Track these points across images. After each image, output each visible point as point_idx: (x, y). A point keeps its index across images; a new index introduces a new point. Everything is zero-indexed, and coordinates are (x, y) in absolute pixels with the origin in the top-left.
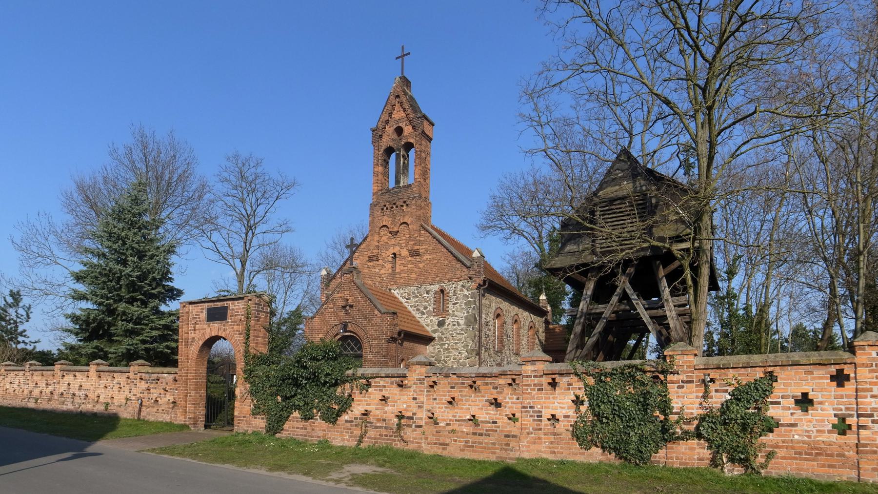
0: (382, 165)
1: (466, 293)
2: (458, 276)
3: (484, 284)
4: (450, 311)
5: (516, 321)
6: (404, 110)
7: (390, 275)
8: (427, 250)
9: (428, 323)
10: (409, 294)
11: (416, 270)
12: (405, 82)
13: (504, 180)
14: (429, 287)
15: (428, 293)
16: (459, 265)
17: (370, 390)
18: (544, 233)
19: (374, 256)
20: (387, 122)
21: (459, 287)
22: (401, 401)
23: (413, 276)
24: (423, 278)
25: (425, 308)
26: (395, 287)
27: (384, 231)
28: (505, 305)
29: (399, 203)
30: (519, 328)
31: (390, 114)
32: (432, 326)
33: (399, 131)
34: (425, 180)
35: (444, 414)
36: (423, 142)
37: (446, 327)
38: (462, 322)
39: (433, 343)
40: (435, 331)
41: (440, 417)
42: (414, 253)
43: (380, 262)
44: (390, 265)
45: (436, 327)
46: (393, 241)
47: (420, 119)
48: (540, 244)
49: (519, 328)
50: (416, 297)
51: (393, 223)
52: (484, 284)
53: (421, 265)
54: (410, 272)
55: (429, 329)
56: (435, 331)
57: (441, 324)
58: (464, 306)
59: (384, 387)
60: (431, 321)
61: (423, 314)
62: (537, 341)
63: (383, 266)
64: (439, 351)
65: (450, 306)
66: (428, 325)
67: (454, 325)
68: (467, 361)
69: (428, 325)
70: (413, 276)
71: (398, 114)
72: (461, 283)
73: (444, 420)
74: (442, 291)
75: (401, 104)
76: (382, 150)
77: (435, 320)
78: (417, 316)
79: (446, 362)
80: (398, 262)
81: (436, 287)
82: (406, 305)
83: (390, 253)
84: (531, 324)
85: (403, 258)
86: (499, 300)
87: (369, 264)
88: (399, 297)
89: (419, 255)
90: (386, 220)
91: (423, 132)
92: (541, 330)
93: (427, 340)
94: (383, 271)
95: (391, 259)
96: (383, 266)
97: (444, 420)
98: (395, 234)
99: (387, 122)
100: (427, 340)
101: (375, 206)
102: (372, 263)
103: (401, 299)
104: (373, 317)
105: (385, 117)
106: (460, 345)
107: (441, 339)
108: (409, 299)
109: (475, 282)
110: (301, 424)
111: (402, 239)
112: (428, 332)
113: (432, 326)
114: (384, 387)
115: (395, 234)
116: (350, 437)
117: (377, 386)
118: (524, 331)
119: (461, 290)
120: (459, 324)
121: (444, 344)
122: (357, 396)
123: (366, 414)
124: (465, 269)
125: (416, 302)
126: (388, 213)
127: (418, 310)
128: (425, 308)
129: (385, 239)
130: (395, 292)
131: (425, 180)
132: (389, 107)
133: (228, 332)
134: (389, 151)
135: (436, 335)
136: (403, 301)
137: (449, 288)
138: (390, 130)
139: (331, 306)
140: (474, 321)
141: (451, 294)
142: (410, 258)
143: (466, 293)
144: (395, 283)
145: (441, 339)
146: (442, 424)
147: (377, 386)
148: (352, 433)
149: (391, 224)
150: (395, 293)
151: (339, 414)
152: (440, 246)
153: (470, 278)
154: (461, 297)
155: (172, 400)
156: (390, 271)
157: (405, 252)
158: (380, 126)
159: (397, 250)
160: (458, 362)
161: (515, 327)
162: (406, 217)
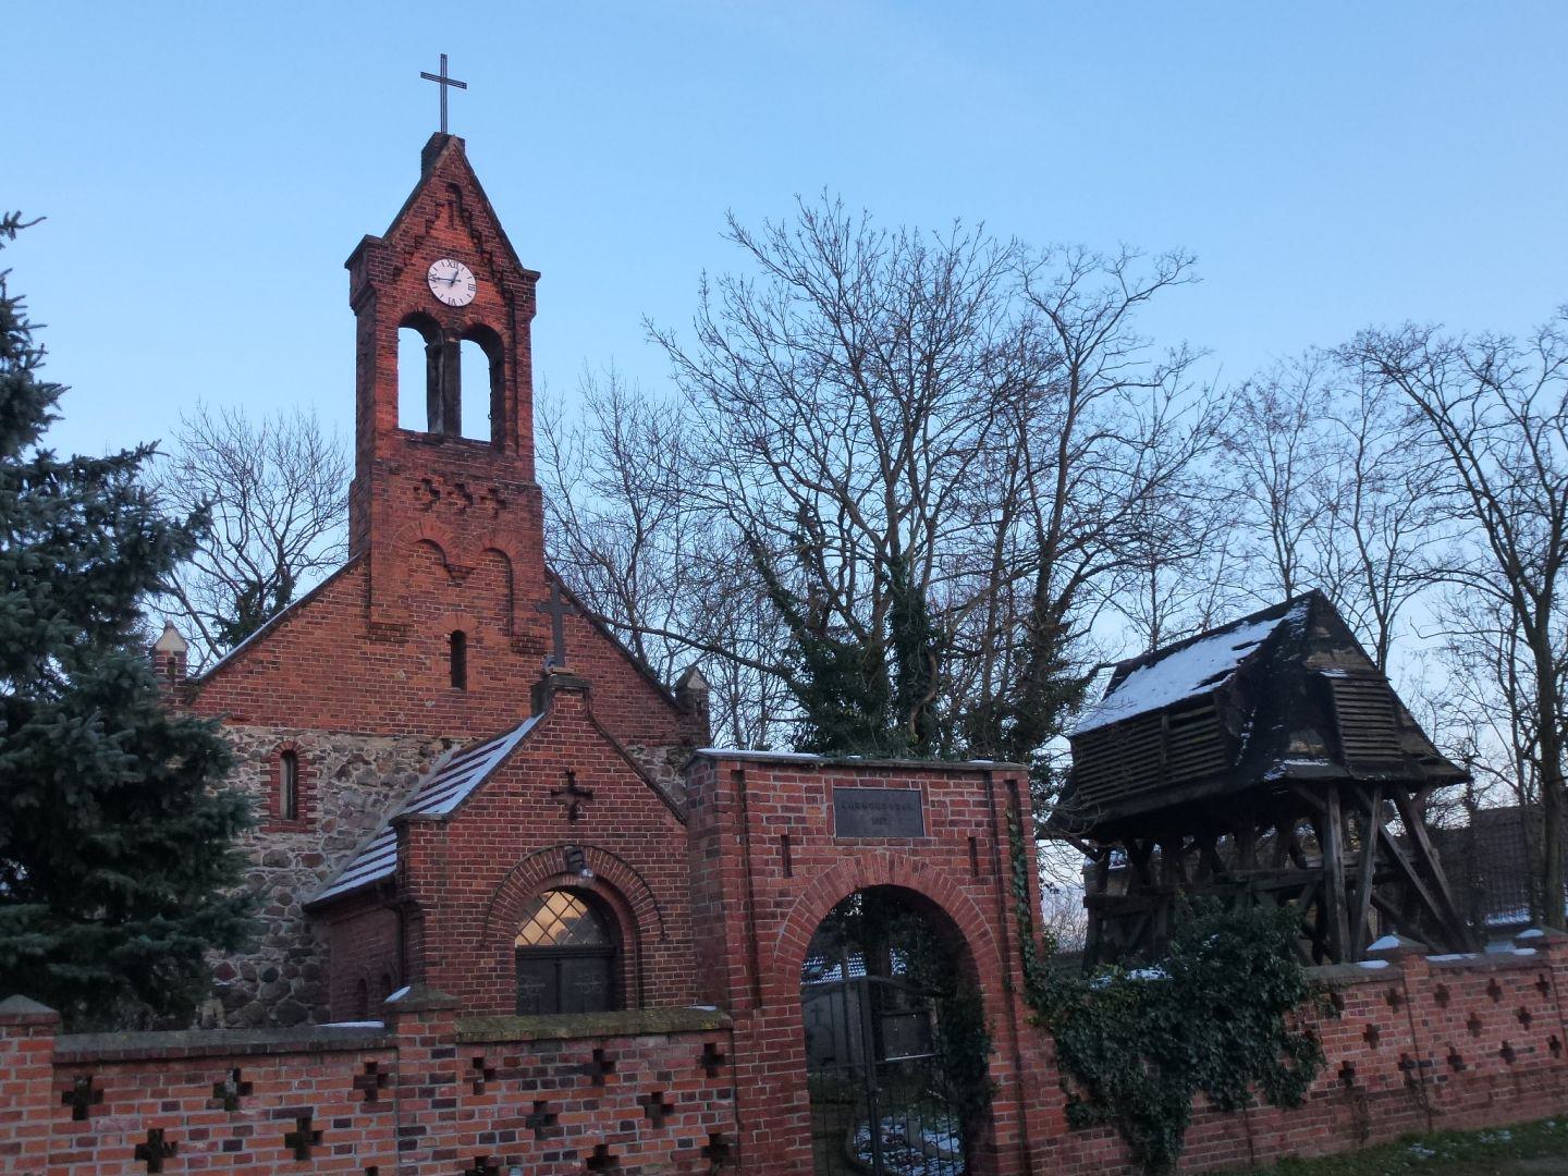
2: (658, 732)
17: (1343, 1013)
19: (393, 628)
22: (1502, 1027)
35: (1466, 1045)
41: (1465, 1054)
46: (452, 595)
59: (1367, 1004)
73: (1473, 1059)
87: (367, 647)
94: (419, 680)
97: (1473, 1059)
102: (379, 648)
110: (1218, 1124)
114: (1367, 1004)
116: (1333, 1130)
117: (1354, 1005)
122: (1323, 1027)
123: (1347, 1072)
133: (931, 873)
139: (513, 786)
142: (512, 658)
146: (1471, 1068)
147: (1354, 1005)
148: (1334, 1120)
151: (1300, 1079)
155: (701, 1139)
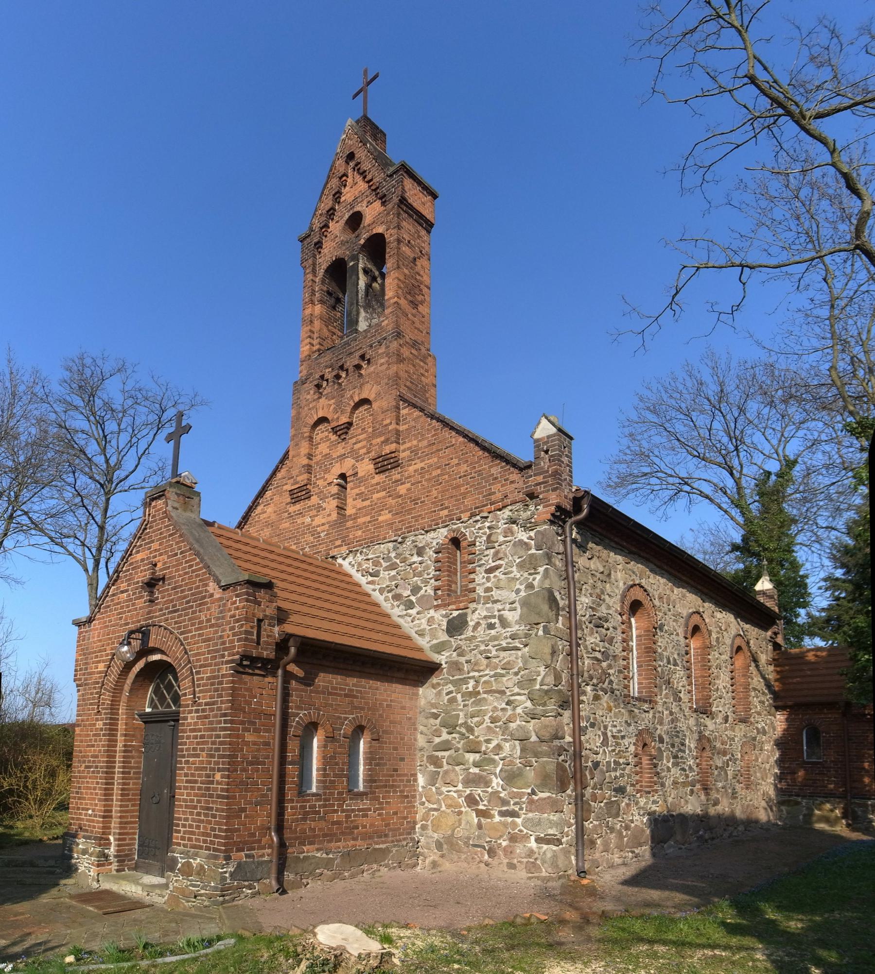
0: (321, 302)
1: (523, 536)
3: (577, 509)
4: (480, 591)
5: (696, 629)
6: (363, 174)
7: (333, 525)
8: (414, 451)
9: (421, 628)
10: (376, 563)
11: (391, 501)
12: (370, 129)
13: (647, 393)
14: (422, 540)
15: (420, 552)
16: (497, 469)
18: (749, 485)
20: (331, 213)
21: (502, 526)
23: (385, 517)
24: (408, 521)
25: (415, 590)
26: (344, 550)
27: (322, 432)
28: (657, 584)
29: (350, 363)
30: (707, 648)
31: (337, 196)
32: (433, 636)
33: (355, 221)
34: (414, 304)
36: (404, 224)
37: (469, 633)
38: (512, 616)
39: (434, 680)
40: (439, 648)
42: (385, 464)
43: (314, 500)
44: (334, 503)
45: (444, 637)
47: (398, 182)
48: (739, 503)
49: (707, 648)
50: (393, 567)
51: (339, 408)
52: (577, 509)
53: (402, 489)
54: (376, 509)
55: (424, 642)
56: (439, 648)
57: (456, 627)
58: (515, 572)
60: (430, 621)
61: (410, 605)
62: (757, 682)
63: (319, 508)
64: (453, 700)
65: (480, 577)
66: (421, 634)
67: (491, 626)
68: (532, 725)
69: (421, 634)
70: (385, 517)
71: (354, 189)
72: (507, 513)
74: (456, 542)
75: (357, 168)
76: (321, 273)
77: (440, 617)
78: (396, 611)
79: (470, 730)
80: (352, 492)
81: (441, 535)
82: (368, 588)
83: (332, 476)
84: (738, 642)
85: (362, 480)
86: (638, 567)
88: (353, 572)
89: (396, 465)
90: (324, 407)
91: (403, 201)
92: (763, 658)
93: (419, 671)
94: (318, 520)
95: (335, 489)
96: (319, 508)
98: (343, 431)
99: (331, 213)
100: (419, 671)
101: (303, 383)
102: (298, 507)
103: (358, 577)
104: (202, 599)
105: (327, 203)
106: (509, 681)
107: (456, 666)
108: (375, 574)
109: (544, 501)
111: (358, 439)
112: (420, 650)
113: (433, 636)
115: (343, 431)
118: (720, 656)
119: (508, 532)
120: (504, 623)
121: (465, 681)
124: (515, 476)
125: (393, 578)
126: (328, 390)
127: (397, 597)
128: (415, 590)
129: (323, 448)
130: (345, 564)
131: (414, 304)
132: (334, 183)
134: (339, 272)
135: (441, 658)
136: (363, 580)
137: (474, 531)
138: (336, 227)
140: (551, 605)
141: (480, 545)
142: (378, 478)
143: (523, 536)
144: (345, 541)
145: (456, 666)
149: (335, 411)
150: (346, 564)
152: (447, 434)
153: (532, 496)
154: (507, 549)
156: (334, 516)
157: (366, 467)
158: (317, 225)
159: (346, 466)
160: (505, 729)
161: (694, 644)
162: (367, 387)
